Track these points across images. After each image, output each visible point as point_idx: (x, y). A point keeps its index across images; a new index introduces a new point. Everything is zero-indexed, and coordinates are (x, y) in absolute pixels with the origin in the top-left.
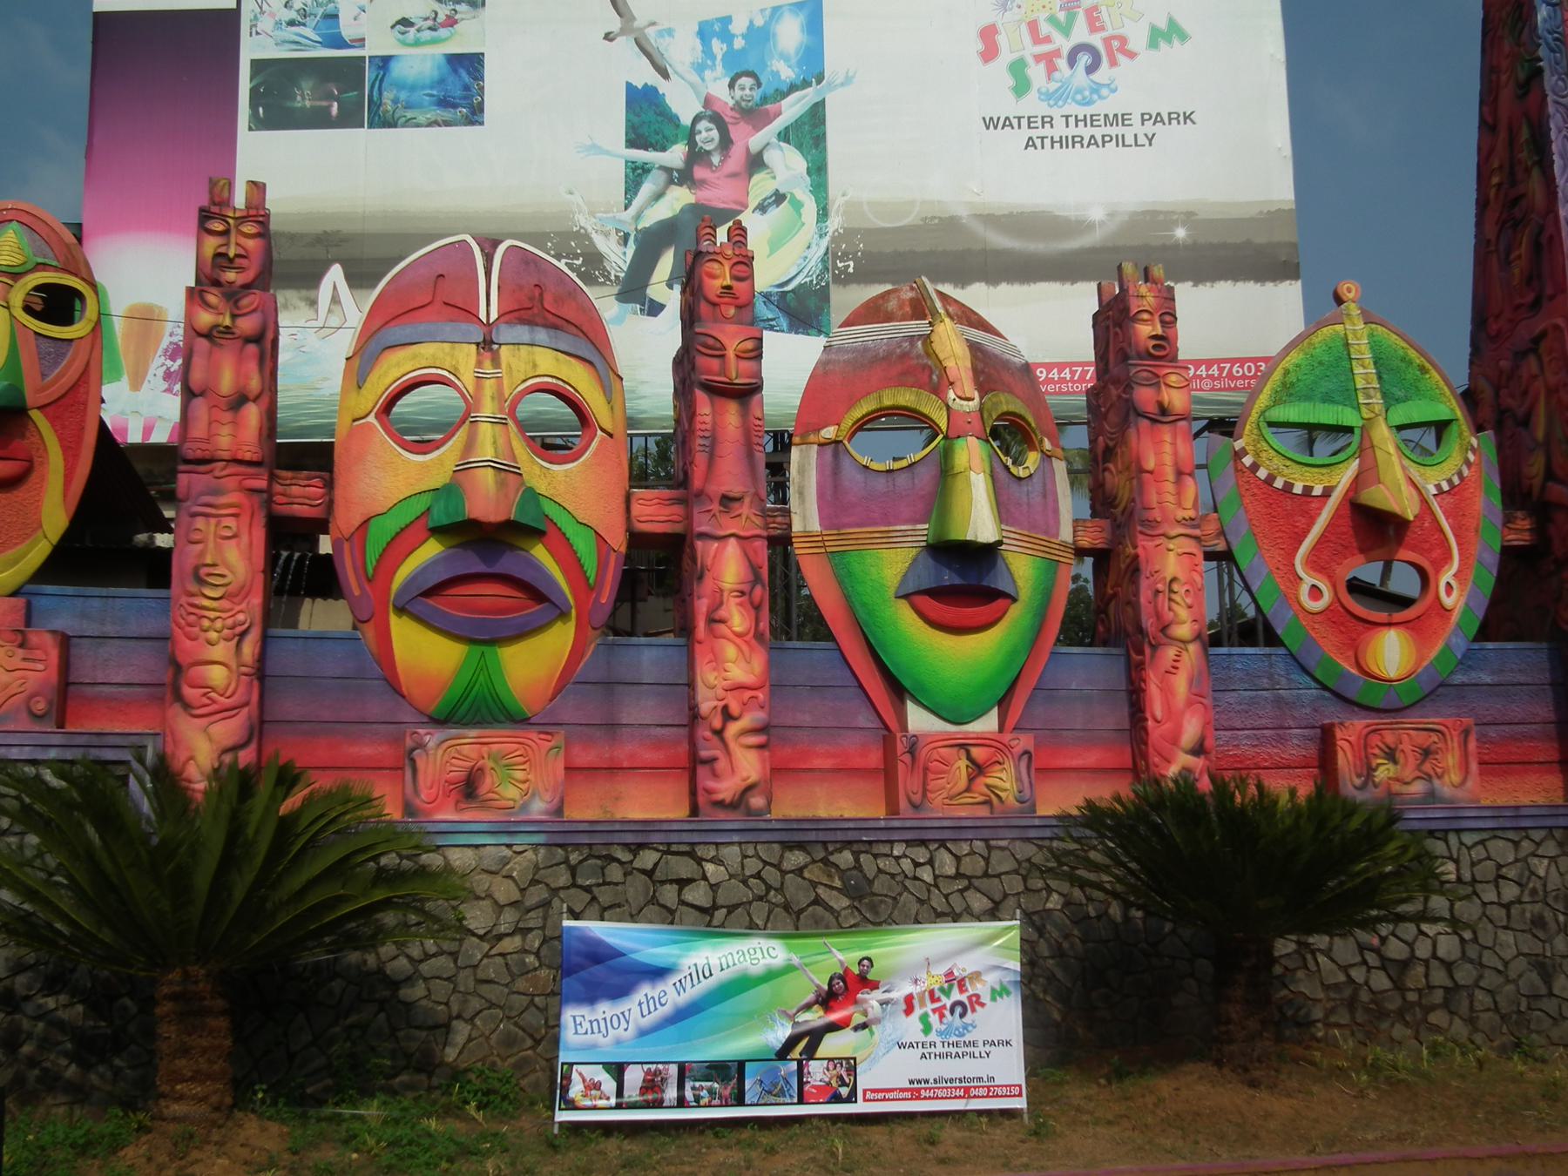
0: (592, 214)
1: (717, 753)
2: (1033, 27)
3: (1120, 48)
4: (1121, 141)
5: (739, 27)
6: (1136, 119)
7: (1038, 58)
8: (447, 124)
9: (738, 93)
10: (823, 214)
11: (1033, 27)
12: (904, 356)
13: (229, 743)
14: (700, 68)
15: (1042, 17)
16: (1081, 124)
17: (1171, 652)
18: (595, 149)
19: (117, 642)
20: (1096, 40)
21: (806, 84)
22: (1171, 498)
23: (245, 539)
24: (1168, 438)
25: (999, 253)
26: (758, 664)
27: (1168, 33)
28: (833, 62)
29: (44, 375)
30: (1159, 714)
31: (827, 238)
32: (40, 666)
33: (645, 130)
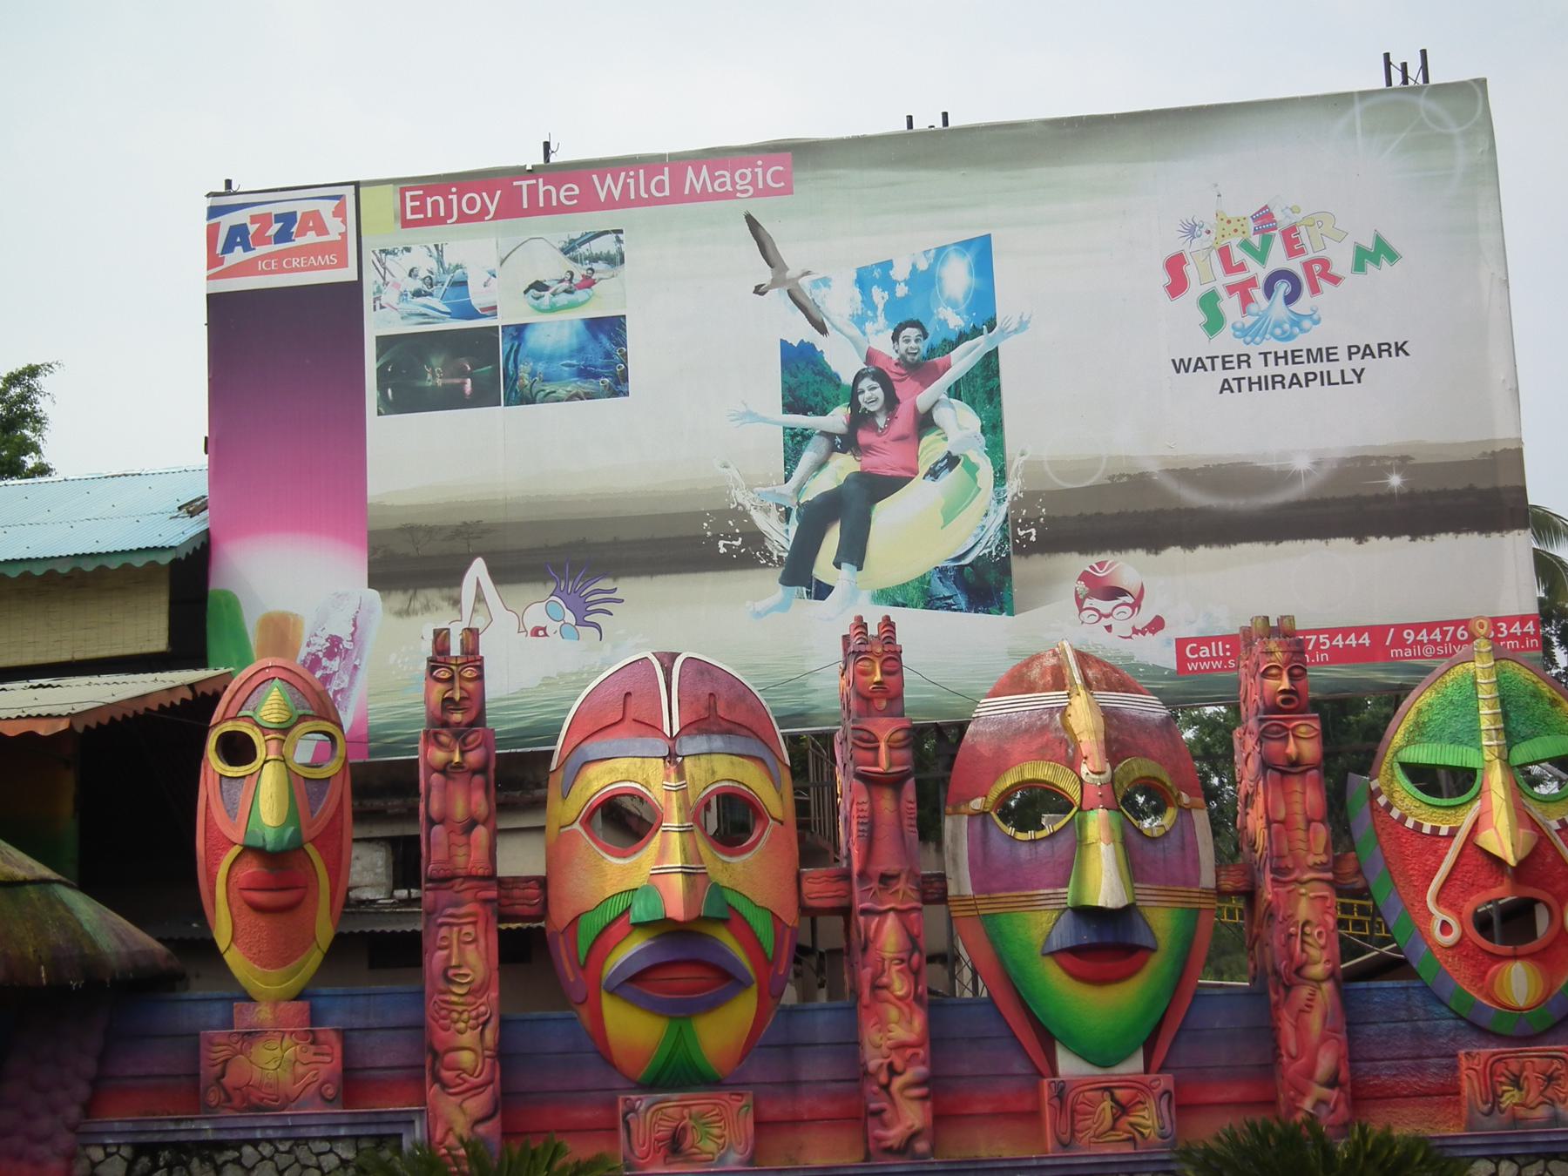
0: (750, 488)
1: (884, 1105)
2: (1225, 253)
3: (1322, 271)
4: (1326, 379)
5: (900, 272)
6: (1342, 353)
7: (1231, 289)
8: (589, 396)
9: (903, 346)
10: (1001, 476)
11: (1225, 253)
12: (1044, 729)
13: (479, 1114)
14: (860, 320)
15: (1234, 242)
16: (1281, 361)
17: (1305, 992)
18: (750, 416)
19: (380, 1033)
20: (1295, 265)
21: (976, 332)
22: (1302, 845)
23: (482, 942)
24: (1298, 788)
25: (1193, 513)
26: (918, 1023)
27: (1376, 253)
28: (1004, 311)
29: (312, 813)
30: (1293, 1050)
31: (1006, 504)
32: (328, 1059)
33: (802, 393)
